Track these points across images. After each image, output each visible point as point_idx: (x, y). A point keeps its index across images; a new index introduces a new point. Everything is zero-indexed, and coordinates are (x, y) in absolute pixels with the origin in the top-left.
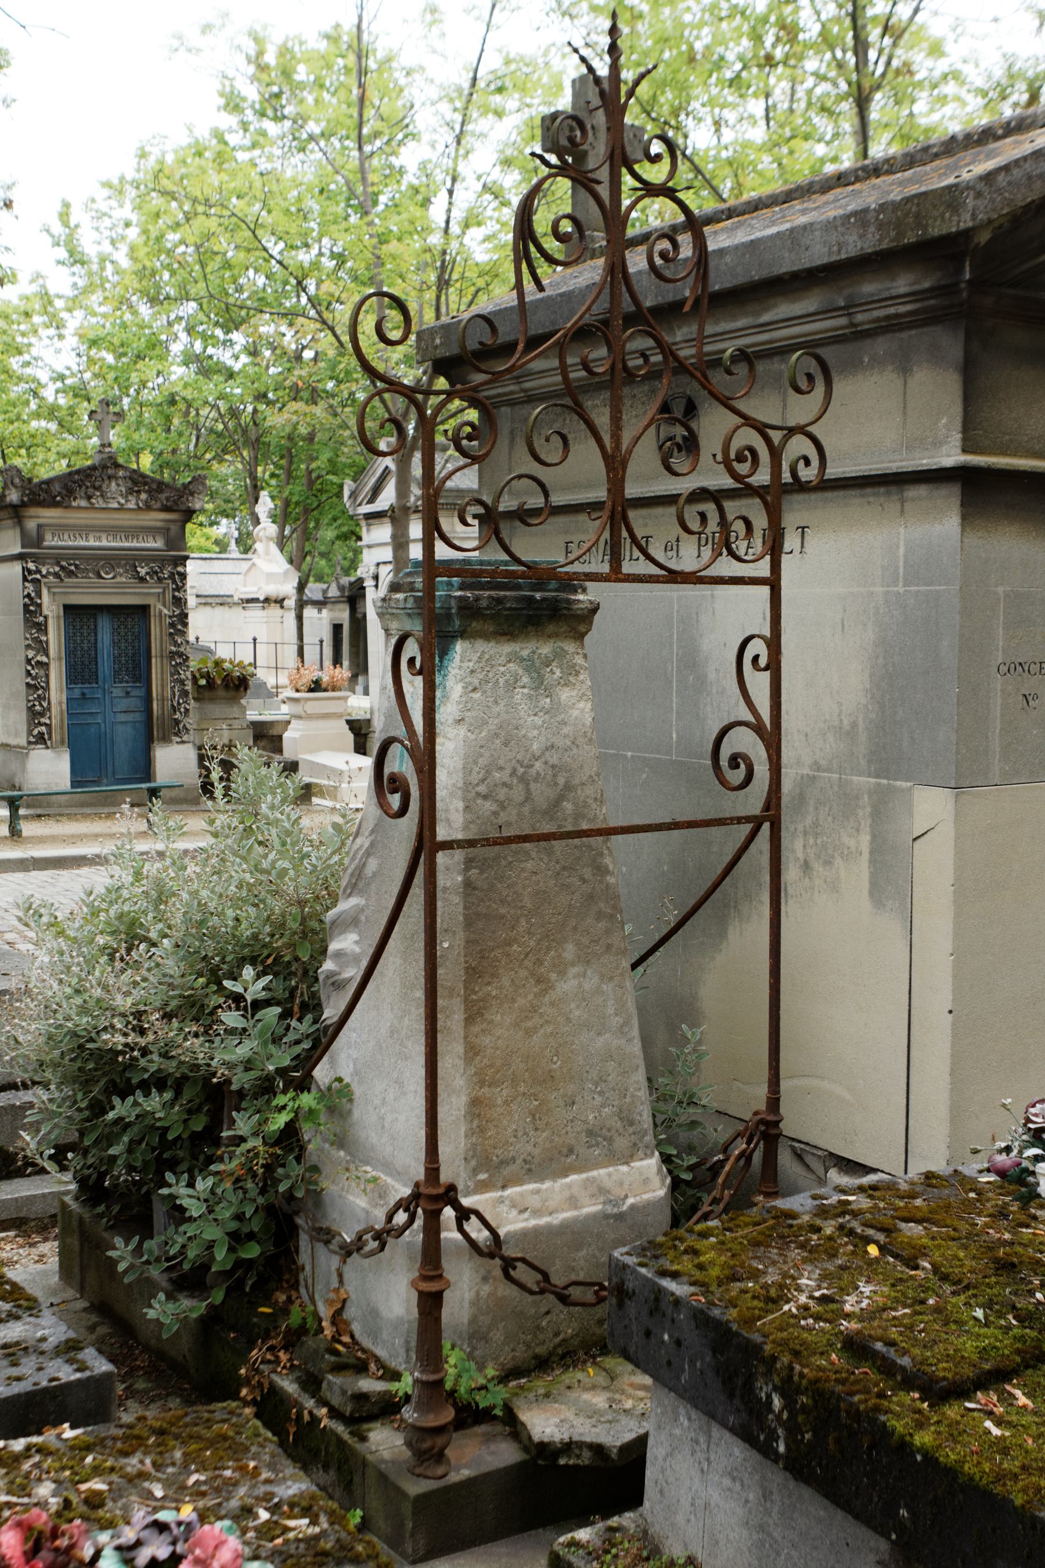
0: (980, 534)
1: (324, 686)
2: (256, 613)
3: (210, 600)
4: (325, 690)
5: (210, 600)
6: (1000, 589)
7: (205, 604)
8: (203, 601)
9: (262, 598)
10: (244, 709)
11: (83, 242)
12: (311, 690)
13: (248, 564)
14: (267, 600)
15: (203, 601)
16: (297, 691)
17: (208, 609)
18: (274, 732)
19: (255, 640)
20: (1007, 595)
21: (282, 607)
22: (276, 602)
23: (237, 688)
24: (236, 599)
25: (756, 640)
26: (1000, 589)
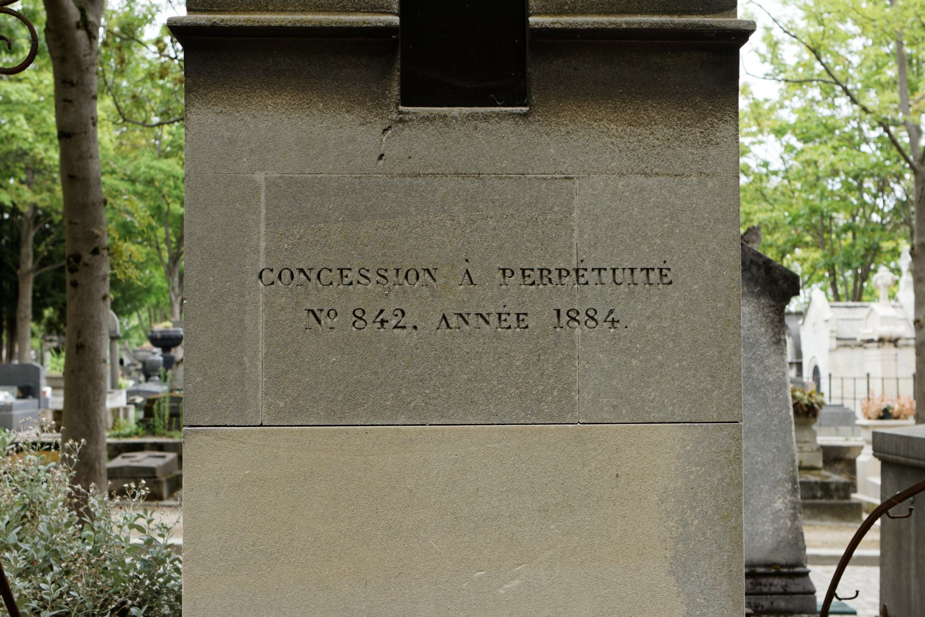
0: (219, 109)
1: (895, 414)
2: (873, 353)
3: (849, 342)
4: (897, 418)
5: (849, 342)
6: (260, 177)
7: (845, 346)
8: (843, 343)
9: (876, 338)
10: (814, 435)
11: (785, 56)
12: (880, 418)
13: (866, 311)
14: (881, 340)
15: (843, 343)
16: (869, 418)
17: (848, 350)
18: (850, 456)
19: (868, 375)
20: (270, 183)
21: (896, 346)
22: (890, 341)
23: (806, 415)
24: (859, 340)
25: (264, 273)
26: (260, 177)
